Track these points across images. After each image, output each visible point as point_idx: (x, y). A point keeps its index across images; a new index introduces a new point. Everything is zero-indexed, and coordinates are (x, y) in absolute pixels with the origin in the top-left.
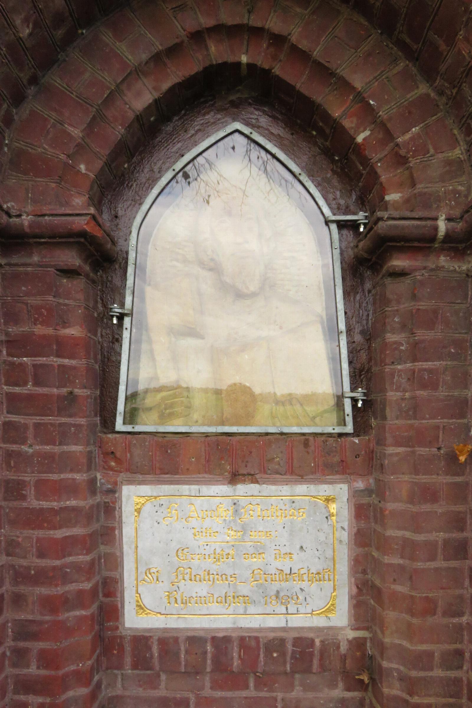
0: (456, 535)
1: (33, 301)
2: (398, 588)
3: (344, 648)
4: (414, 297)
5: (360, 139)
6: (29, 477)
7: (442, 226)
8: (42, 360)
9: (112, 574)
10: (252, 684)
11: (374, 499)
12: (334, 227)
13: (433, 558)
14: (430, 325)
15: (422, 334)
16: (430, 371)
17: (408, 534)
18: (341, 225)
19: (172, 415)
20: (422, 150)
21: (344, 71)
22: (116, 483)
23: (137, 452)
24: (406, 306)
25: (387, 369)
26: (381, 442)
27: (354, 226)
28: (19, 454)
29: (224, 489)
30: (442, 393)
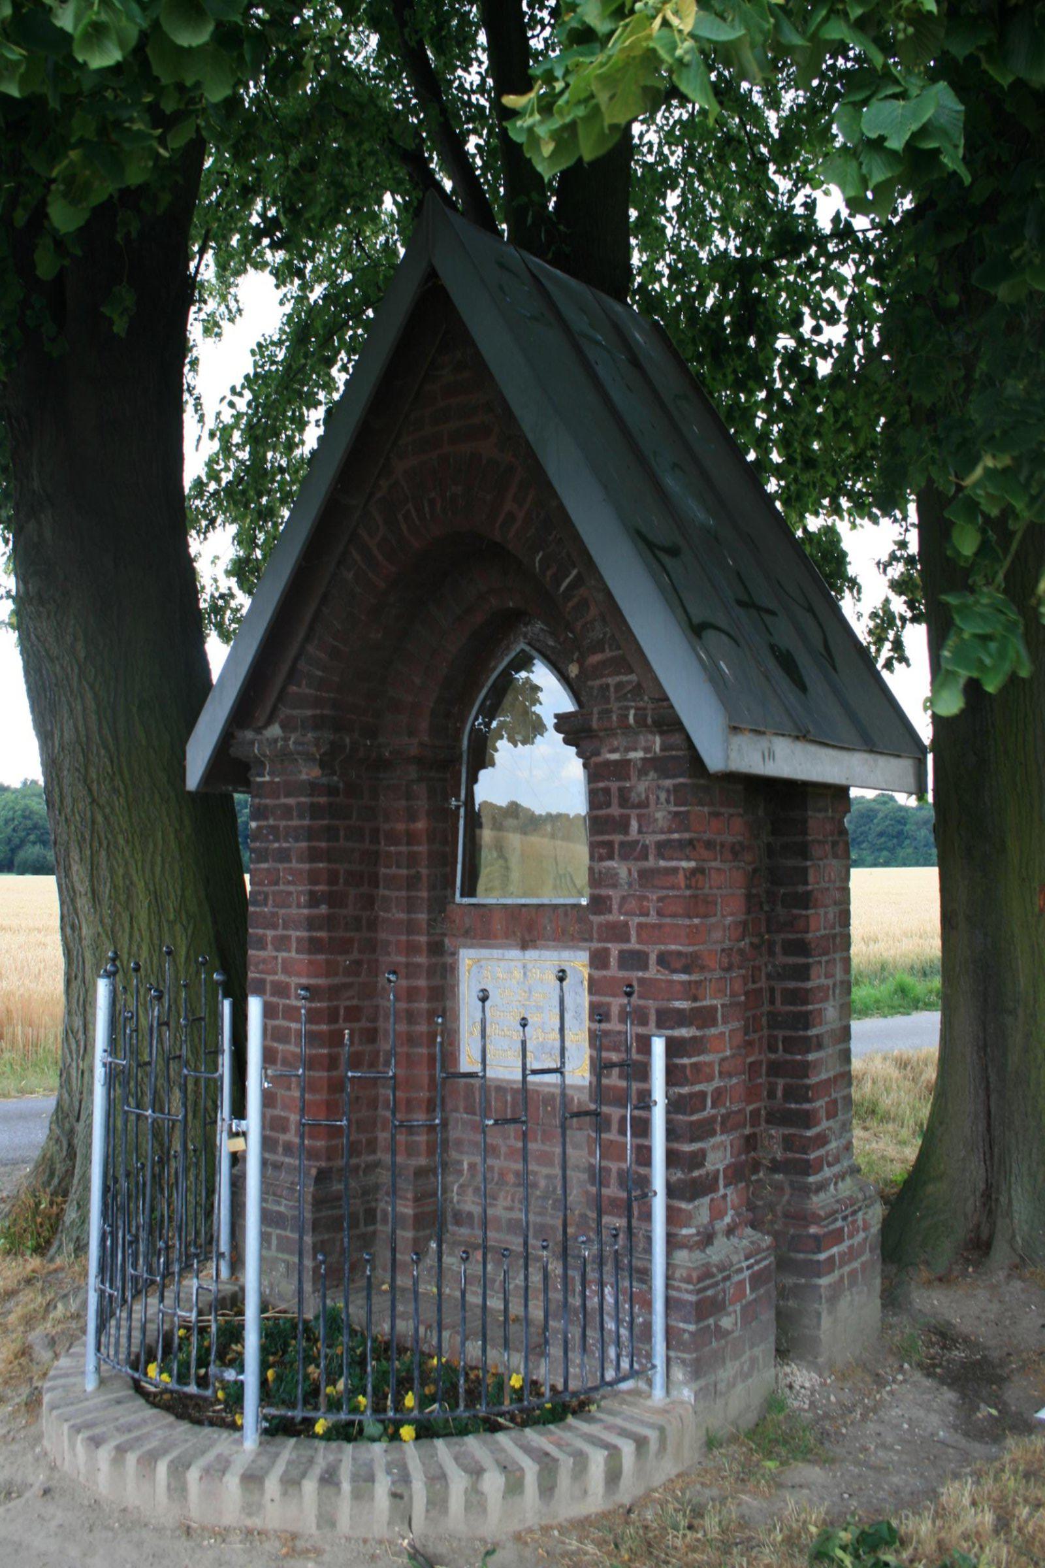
29: (515, 953)
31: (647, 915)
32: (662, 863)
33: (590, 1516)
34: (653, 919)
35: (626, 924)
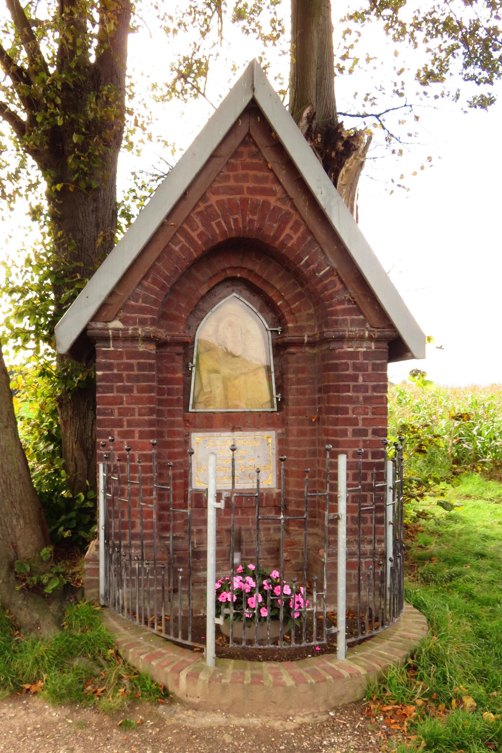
0: (312, 448)
1: (168, 365)
2: (294, 469)
3: (274, 496)
4: (297, 362)
5: (279, 304)
6: (165, 429)
7: (306, 339)
8: (170, 386)
9: (187, 469)
10: (240, 513)
11: (285, 437)
12: (269, 332)
13: (305, 456)
14: (303, 372)
15: (300, 376)
16: (303, 389)
17: (296, 448)
18: (271, 331)
19: (209, 405)
20: (299, 311)
21: (273, 282)
22: (189, 432)
23: (197, 420)
24: (295, 365)
25: (289, 387)
26: (287, 414)
27: (277, 331)
28: (162, 421)
29: (229, 434)
30: (307, 396)
31: (367, 414)
32: (375, 394)
33: (336, 642)
34: (370, 416)
35: (357, 418)
